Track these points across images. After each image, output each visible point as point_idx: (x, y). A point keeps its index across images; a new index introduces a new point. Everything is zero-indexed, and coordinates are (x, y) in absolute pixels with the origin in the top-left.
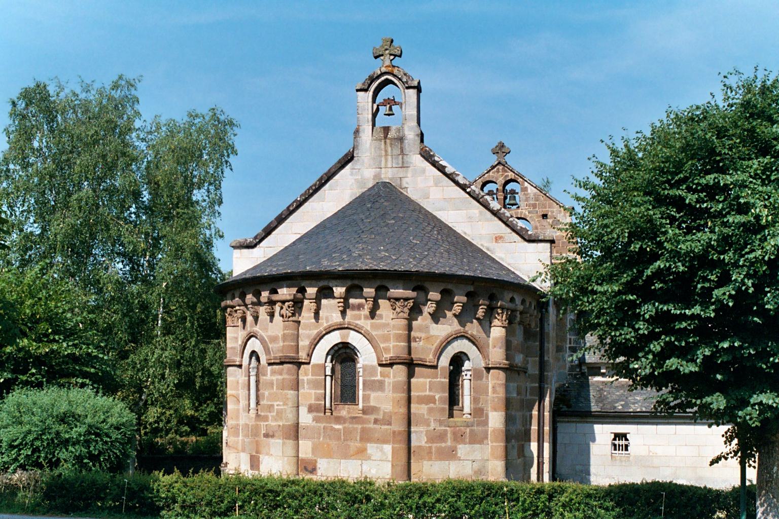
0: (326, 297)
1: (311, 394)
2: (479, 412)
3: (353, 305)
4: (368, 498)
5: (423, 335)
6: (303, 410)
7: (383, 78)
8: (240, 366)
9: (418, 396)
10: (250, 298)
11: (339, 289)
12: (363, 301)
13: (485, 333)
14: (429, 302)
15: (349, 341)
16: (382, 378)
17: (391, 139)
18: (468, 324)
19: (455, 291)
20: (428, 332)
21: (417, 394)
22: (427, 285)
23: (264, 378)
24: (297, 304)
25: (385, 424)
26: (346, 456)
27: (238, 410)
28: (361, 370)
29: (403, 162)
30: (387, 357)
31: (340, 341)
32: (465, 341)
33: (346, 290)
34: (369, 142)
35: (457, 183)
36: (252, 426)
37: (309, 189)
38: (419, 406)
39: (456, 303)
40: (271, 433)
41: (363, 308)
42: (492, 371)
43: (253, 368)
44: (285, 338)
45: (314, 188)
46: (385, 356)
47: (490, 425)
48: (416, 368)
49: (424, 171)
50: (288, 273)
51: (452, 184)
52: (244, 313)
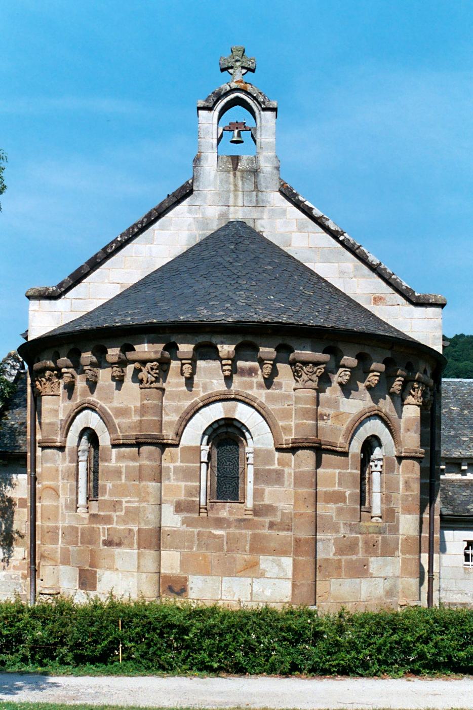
0: (203, 358)
1: (179, 487)
2: (389, 515)
3: (241, 368)
4: (318, 635)
5: (332, 412)
7: (232, 96)
8: (62, 449)
9: (325, 493)
10: (87, 357)
11: (225, 347)
12: (256, 364)
13: (397, 412)
14: (341, 370)
15: (237, 417)
16: (279, 468)
17: (242, 171)
18: (381, 400)
19: (373, 357)
20: (337, 407)
21: (324, 489)
22: (341, 346)
23: (106, 464)
24: (163, 366)
25: (284, 530)
26: (229, 572)
27: (57, 507)
28: (251, 456)
29: (257, 201)
30: (288, 438)
31: (223, 416)
32: (378, 422)
33: (235, 349)
34: (213, 173)
35: (327, 229)
36: (83, 529)
37: (133, 228)
38: (327, 505)
39: (373, 371)
40: (116, 540)
41: (256, 374)
42: (404, 461)
43: (84, 451)
44: (143, 410)
45: (140, 226)
47: (401, 532)
48: (324, 455)
49: (284, 212)
50: (152, 323)
51: (321, 230)
52: (73, 377)
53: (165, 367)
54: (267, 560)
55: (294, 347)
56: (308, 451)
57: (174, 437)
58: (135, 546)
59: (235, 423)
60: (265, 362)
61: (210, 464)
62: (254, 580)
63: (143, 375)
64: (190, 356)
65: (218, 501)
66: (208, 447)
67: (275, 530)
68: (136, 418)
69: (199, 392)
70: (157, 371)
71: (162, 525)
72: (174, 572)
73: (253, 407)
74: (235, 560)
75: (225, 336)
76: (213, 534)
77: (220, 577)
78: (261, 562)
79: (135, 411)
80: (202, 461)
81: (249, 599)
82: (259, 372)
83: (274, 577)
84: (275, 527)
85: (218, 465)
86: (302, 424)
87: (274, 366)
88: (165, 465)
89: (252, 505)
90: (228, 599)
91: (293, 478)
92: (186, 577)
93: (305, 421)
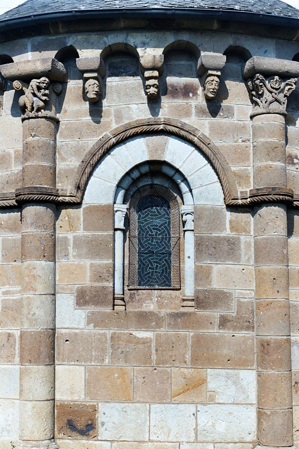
1: (82, 267)
3: (173, 86)
6: (66, 302)
12: (195, 81)
16: (233, 234)
24: (56, 83)
25: (241, 329)
26: (162, 397)
30: (244, 191)
31: (146, 158)
41: (195, 94)
44: (28, 151)
46: (240, 189)
53: (59, 87)
54: (218, 375)
55: (251, 52)
56: (276, 208)
57: (74, 192)
58: (17, 359)
59: (166, 170)
60: (210, 72)
61: (128, 233)
62: (200, 407)
63: (26, 99)
64: (96, 65)
65: (141, 287)
66: (126, 206)
67: (229, 329)
68: (16, 168)
69: (110, 123)
70: (47, 92)
71: (57, 326)
72: (76, 398)
73: (191, 143)
74: (170, 377)
75: (148, 34)
76: (135, 337)
77: (148, 405)
78: (209, 379)
79: (16, 158)
80: (116, 227)
81: (192, 439)
82: (200, 91)
83: (230, 402)
84: (228, 324)
85: (139, 234)
86: (266, 167)
87: (222, 79)
88: (61, 235)
89: (193, 292)
90: (158, 439)
91: (253, 249)
92: (94, 406)
93: (270, 163)
